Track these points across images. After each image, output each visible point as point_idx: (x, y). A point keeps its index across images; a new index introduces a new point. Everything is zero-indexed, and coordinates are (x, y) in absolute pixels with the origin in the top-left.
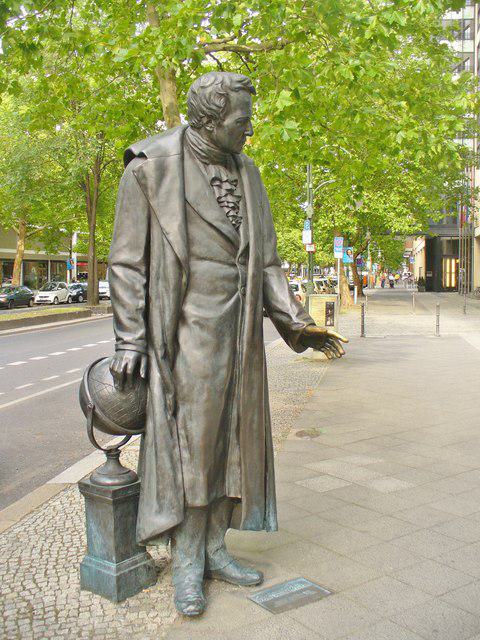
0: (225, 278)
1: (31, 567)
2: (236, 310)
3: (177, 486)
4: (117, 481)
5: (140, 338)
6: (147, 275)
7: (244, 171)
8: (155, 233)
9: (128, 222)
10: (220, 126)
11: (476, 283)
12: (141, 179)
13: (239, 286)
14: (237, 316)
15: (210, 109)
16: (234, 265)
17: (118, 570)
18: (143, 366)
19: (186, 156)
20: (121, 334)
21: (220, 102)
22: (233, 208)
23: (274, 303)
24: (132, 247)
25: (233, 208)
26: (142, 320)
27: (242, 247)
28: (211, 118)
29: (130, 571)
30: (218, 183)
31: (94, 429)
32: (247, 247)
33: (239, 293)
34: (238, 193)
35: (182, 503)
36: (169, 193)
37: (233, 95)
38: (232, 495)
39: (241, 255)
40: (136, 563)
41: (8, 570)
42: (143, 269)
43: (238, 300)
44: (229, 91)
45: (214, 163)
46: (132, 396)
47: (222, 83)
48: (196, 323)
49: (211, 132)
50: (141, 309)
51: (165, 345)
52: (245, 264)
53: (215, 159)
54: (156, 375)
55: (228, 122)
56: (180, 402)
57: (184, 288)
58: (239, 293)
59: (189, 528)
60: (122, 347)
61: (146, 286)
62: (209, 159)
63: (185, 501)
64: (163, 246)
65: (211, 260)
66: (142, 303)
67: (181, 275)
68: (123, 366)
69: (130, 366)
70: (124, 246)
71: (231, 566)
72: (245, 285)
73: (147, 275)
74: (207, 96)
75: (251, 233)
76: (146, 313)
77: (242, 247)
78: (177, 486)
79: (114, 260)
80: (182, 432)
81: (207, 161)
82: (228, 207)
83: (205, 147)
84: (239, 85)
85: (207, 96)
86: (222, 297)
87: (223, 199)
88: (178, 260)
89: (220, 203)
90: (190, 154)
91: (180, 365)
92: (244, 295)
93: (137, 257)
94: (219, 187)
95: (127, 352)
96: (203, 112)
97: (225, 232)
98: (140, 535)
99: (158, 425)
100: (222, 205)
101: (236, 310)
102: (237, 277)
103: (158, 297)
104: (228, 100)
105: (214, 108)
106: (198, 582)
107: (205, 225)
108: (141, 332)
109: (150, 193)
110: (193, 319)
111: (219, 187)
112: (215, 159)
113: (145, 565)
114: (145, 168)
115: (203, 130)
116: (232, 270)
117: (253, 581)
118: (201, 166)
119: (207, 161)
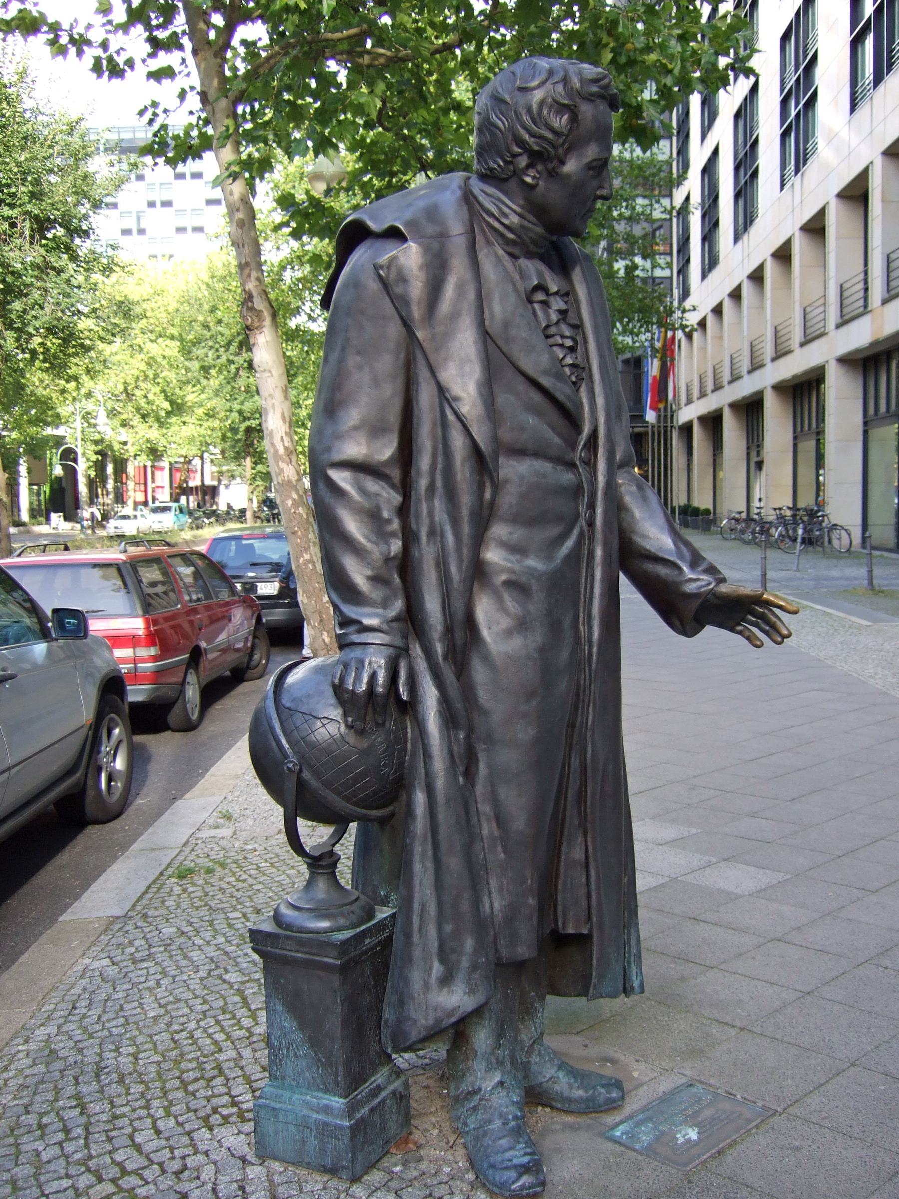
0: (561, 490)
1: (116, 1117)
2: (579, 558)
3: (481, 925)
5: (396, 619)
6: (406, 487)
7: (577, 275)
8: (425, 397)
9: (365, 377)
10: (553, 174)
12: (389, 283)
13: (583, 508)
14: (578, 569)
15: (541, 137)
16: (572, 465)
17: (351, 1109)
18: (402, 677)
19: (480, 239)
20: (350, 611)
21: (561, 122)
22: (572, 349)
23: (637, 539)
24: (375, 430)
25: (572, 349)
26: (397, 579)
27: (586, 430)
28: (536, 157)
30: (540, 296)
31: (300, 821)
32: (594, 433)
33: (582, 522)
34: (572, 317)
37: (586, 110)
38: (571, 930)
39: (584, 446)
40: (379, 1089)
41: (67, 1130)
44: (578, 100)
45: (529, 255)
46: (378, 738)
47: (565, 80)
48: (510, 584)
49: (532, 187)
50: (394, 557)
52: (591, 464)
53: (532, 248)
54: (430, 695)
55: (571, 167)
57: (486, 512)
58: (582, 522)
60: (356, 638)
61: (403, 511)
62: (519, 247)
63: (497, 950)
65: (537, 454)
66: (396, 546)
67: (481, 488)
69: (381, 678)
70: (355, 428)
72: (592, 506)
73: (406, 487)
74: (535, 108)
75: (600, 401)
76: (406, 565)
77: (586, 430)
78: (481, 925)
79: (336, 457)
80: (486, 808)
81: (516, 251)
82: (562, 346)
83: (515, 219)
84: (595, 89)
85: (535, 108)
86: (555, 531)
87: (553, 330)
88: (476, 450)
89: (548, 337)
90: (483, 231)
91: (480, 674)
92: (591, 524)
93: (385, 451)
94: (545, 304)
95: (371, 649)
96: (520, 143)
97: (561, 397)
98: (415, 1021)
99: (440, 797)
100: (551, 341)
101: (579, 558)
102: (578, 490)
103: (432, 533)
104: (575, 118)
105: (549, 135)
107: (522, 386)
108: (398, 606)
110: (504, 577)
111: (545, 304)
112: (532, 248)
113: (394, 1093)
114: (402, 260)
115: (513, 184)
116: (567, 477)
118: (506, 258)
119: (516, 251)
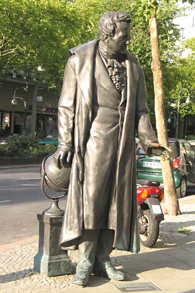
29: (56, 262)
40: (60, 258)
51: (79, 147)
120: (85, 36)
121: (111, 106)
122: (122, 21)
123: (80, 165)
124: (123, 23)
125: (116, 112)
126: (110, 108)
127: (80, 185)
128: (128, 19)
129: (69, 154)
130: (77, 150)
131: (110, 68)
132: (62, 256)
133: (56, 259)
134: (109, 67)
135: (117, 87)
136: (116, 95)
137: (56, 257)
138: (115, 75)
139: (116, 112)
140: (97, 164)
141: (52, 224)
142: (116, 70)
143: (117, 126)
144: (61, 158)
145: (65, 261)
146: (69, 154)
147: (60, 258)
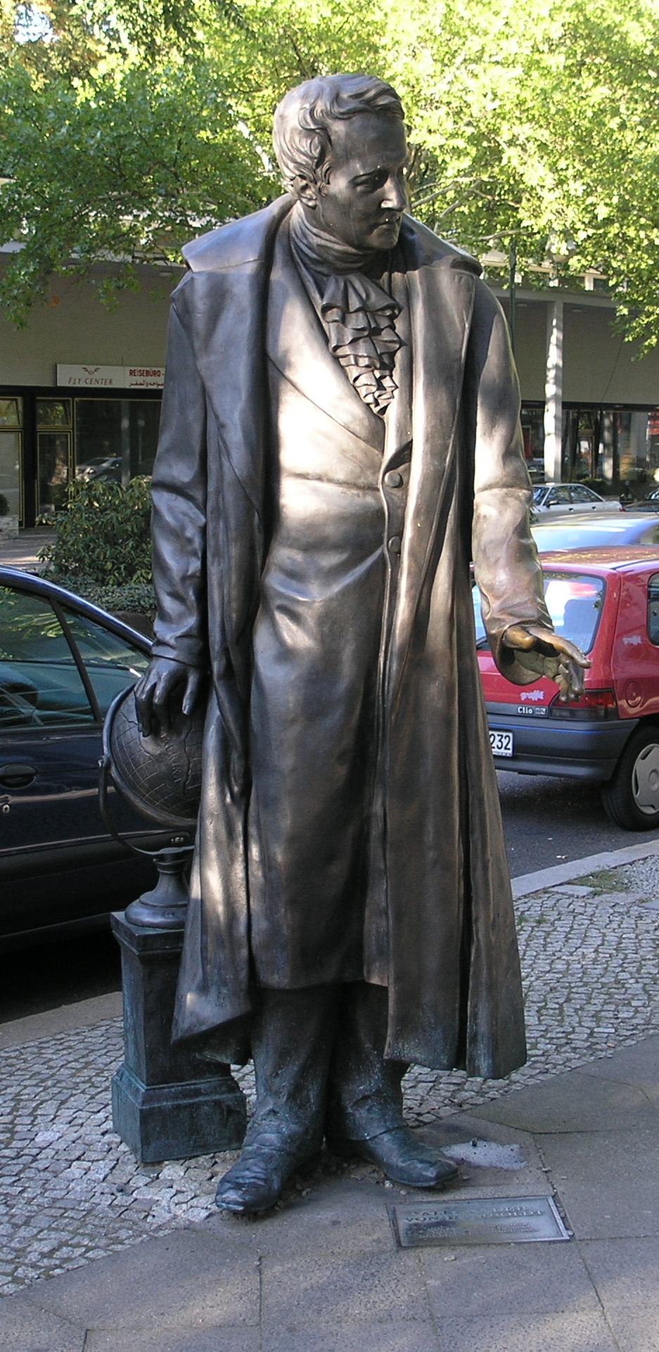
4: (158, 920)
11: (7, 413)
26: (191, 596)
29: (178, 1107)
35: (243, 975)
36: (229, 342)
40: (197, 1093)
42: (199, 495)
43: (382, 561)
50: (192, 576)
51: (225, 651)
56: (254, 768)
59: (272, 1034)
64: (219, 452)
66: (195, 565)
68: (148, 687)
71: (386, 1137)
77: (391, 447)
106: (281, 1150)
108: (191, 621)
109: (197, 344)
112: (339, 264)
117: (421, 1178)
119: (324, 270)
120: (514, 242)
121: (341, 476)
122: (354, 112)
123: (232, 725)
124: (357, 121)
125: (369, 499)
126: (340, 483)
127: (234, 810)
128: (382, 101)
129: (192, 680)
130: (217, 666)
131: (334, 314)
132: (202, 1084)
133: (176, 1096)
134: (325, 309)
135: (363, 391)
136: (357, 429)
137: (176, 1087)
138: (354, 341)
139: (369, 499)
140: (427, 440)
141: (146, 961)
142: (358, 321)
143: (378, 552)
144: (158, 692)
145: (218, 1103)
146: (192, 680)
147: (197, 1093)
